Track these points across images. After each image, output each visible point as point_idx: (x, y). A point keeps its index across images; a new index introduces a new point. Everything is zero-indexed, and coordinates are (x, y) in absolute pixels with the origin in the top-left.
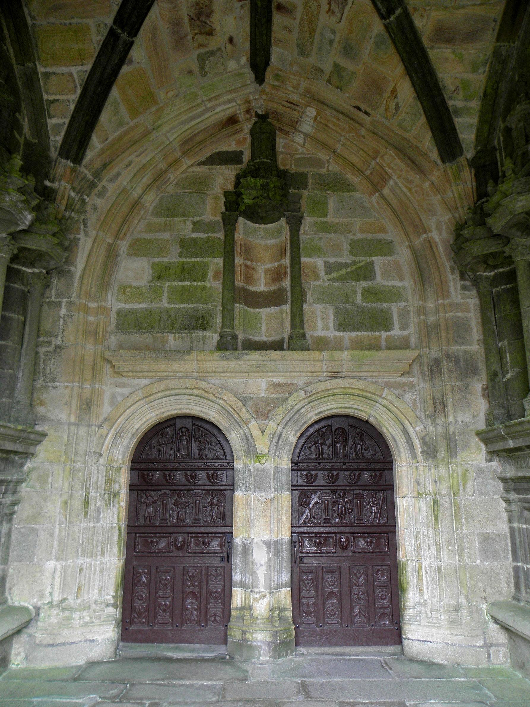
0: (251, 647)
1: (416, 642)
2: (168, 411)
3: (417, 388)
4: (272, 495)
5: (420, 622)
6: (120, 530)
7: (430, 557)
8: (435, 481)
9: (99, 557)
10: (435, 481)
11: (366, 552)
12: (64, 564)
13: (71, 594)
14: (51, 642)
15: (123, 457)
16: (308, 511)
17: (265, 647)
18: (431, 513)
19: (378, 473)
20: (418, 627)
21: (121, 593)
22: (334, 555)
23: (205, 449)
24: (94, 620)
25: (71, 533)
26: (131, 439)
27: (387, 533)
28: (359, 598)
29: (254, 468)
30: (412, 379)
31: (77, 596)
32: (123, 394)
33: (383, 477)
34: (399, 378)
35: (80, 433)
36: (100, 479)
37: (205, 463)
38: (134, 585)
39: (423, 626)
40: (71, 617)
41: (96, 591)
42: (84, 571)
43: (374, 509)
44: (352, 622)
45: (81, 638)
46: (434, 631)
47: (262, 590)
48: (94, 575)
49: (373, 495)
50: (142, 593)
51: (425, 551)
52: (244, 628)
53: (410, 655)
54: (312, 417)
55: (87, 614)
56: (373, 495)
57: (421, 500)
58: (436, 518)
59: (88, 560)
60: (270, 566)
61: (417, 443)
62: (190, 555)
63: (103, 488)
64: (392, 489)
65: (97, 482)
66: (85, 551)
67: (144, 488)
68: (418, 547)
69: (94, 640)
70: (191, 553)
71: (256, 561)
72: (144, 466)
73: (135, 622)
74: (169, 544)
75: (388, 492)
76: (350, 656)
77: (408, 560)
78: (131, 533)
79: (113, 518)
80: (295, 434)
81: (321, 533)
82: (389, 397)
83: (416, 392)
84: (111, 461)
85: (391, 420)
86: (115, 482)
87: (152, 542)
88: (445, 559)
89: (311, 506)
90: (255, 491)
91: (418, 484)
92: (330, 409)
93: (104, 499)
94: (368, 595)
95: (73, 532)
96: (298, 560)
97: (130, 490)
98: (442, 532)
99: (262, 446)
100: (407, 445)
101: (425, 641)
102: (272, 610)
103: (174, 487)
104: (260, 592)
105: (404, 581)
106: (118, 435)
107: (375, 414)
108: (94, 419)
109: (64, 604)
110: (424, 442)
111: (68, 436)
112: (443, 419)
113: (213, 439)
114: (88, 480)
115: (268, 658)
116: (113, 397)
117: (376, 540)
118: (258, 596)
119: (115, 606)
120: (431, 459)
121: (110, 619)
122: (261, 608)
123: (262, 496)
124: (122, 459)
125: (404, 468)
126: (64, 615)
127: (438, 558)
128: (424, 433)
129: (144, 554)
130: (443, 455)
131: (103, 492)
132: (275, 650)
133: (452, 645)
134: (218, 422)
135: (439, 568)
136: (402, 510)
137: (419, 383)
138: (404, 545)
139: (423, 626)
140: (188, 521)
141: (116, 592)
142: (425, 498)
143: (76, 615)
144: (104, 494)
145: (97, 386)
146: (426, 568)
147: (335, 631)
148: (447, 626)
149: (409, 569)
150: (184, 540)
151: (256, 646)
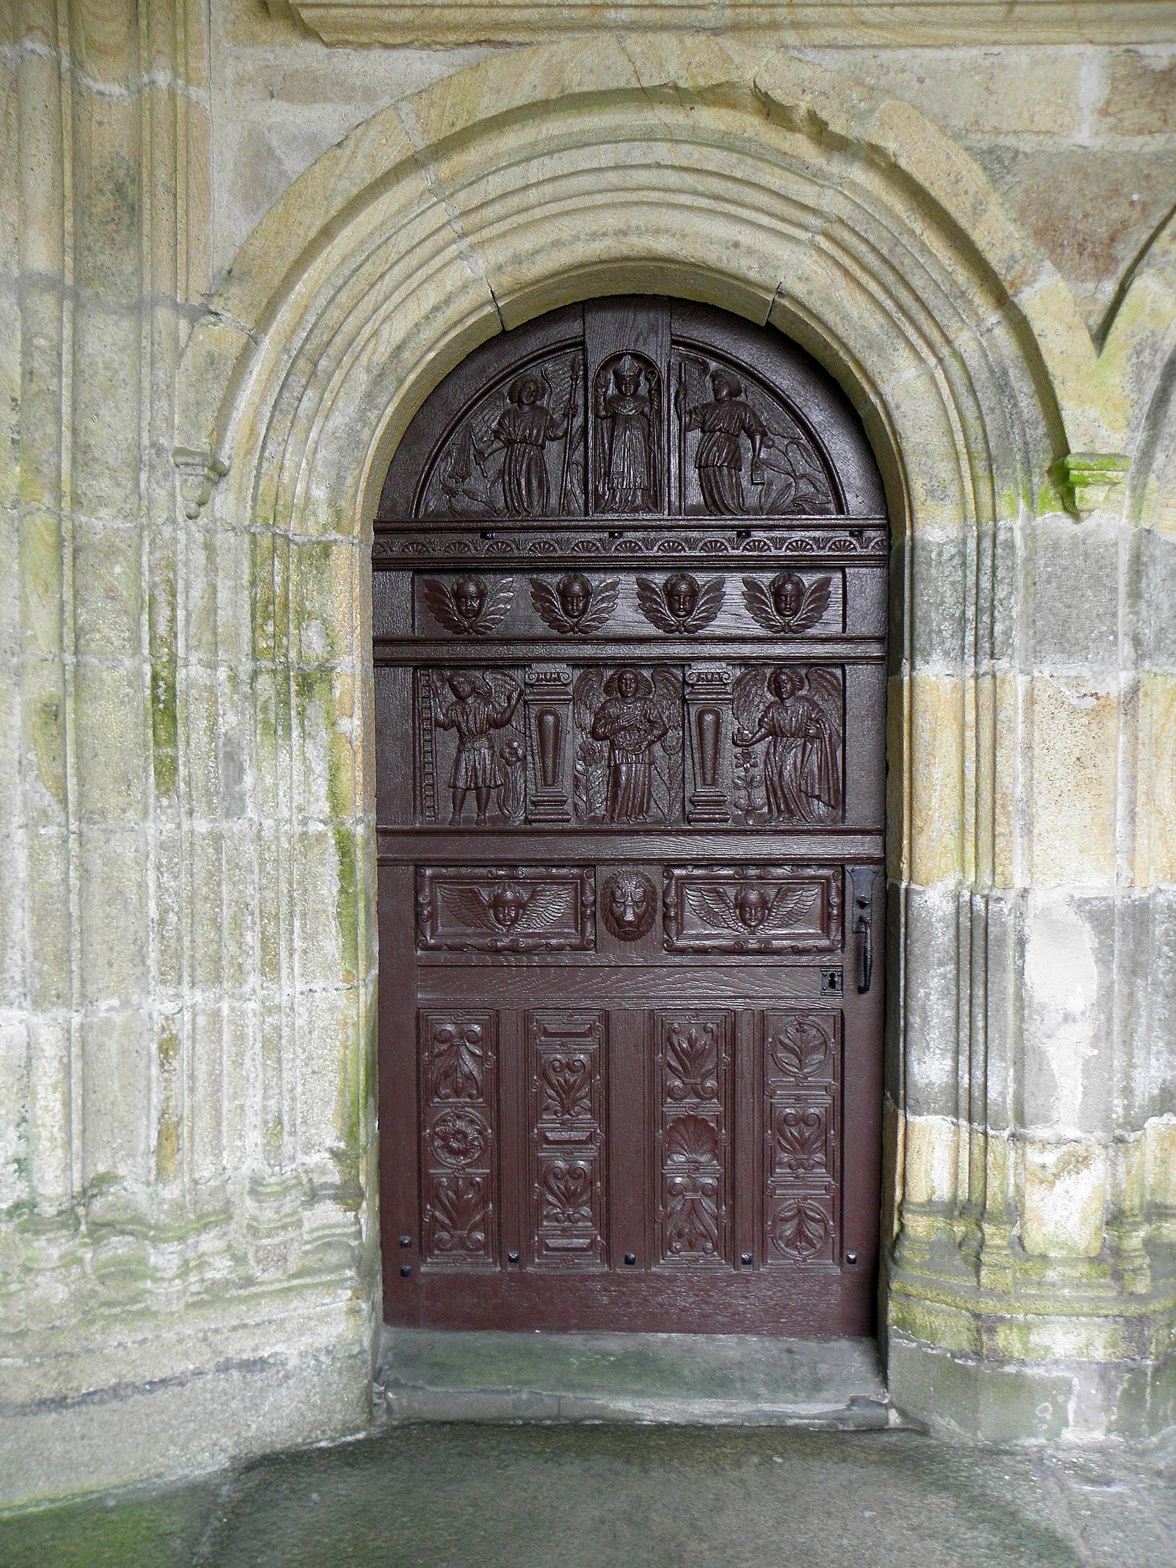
0: (1019, 1384)
2: (556, 244)
6: (345, 848)
9: (253, 980)
12: (77, 1019)
13: (131, 1155)
14: (49, 1390)
15: (336, 490)
17: (1085, 1392)
21: (368, 1129)
23: (735, 463)
24: (257, 1272)
25: (97, 866)
26: (369, 396)
29: (1031, 536)
31: (160, 1170)
32: (313, 140)
35: (92, 346)
36: (223, 596)
37: (744, 532)
38: (425, 1091)
40: (142, 1261)
41: (254, 1137)
42: (185, 1052)
45: (203, 1358)
47: (1072, 1133)
48: (238, 1064)
50: (460, 1124)
52: (987, 1306)
55: (221, 1245)
59: (199, 997)
62: (678, 959)
63: (247, 648)
65: (212, 610)
66: (178, 955)
67: (444, 652)
69: (262, 1361)
70: (682, 951)
72: (439, 546)
73: (439, 1244)
74: (579, 913)
78: (396, 862)
79: (309, 789)
84: (273, 509)
86: (303, 615)
87: (498, 903)
90: (1036, 654)
93: (254, 695)
95: (111, 861)
97: (380, 663)
99: (1093, 413)
102: (1116, 1219)
103: (588, 651)
104: (1059, 1142)
106: (302, 364)
108: (165, 267)
109: (97, 1205)
111: (27, 353)
113: (770, 415)
114: (162, 598)
115: (1098, 1436)
116: (259, 155)
118: (1050, 1158)
119: (347, 1195)
121: (333, 1257)
122: (1064, 1211)
124: (332, 503)
126: (105, 1255)
129: (463, 958)
131: (246, 667)
132: (1133, 1399)
134: (828, 301)
140: (662, 803)
141: (351, 1134)
143: (164, 1258)
144: (255, 674)
145: (163, 78)
150: (649, 896)
151: (1041, 1382)
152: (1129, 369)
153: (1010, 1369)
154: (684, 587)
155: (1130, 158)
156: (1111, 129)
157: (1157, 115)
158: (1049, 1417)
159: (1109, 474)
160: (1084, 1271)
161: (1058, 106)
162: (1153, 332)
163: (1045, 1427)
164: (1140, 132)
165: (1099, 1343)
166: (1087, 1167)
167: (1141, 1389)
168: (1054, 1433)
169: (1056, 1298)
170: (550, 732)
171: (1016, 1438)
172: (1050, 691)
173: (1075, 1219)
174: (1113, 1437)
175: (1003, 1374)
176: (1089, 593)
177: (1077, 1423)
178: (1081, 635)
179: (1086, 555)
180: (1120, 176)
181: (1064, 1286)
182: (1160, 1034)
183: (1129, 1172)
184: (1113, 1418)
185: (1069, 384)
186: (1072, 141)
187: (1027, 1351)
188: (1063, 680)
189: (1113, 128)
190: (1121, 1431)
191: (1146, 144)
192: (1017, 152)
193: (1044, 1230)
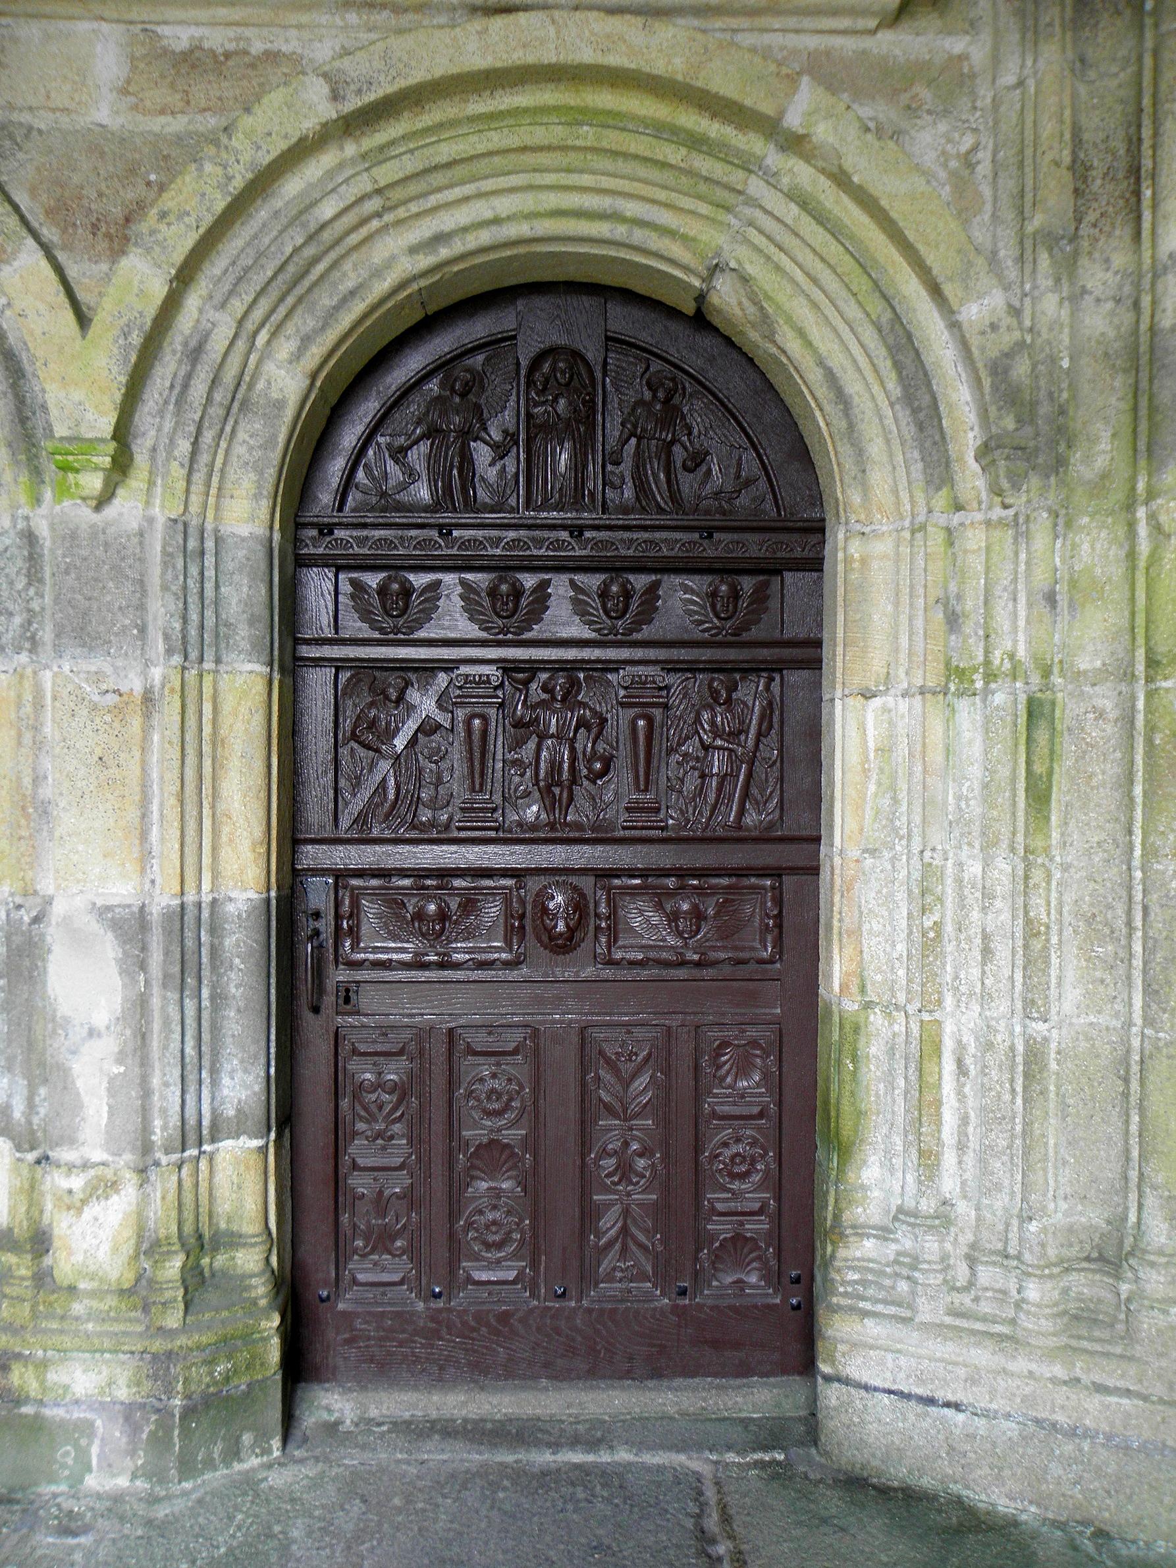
0: (37, 1425)
1: (886, 1399)
3: (985, 95)
4: (157, 673)
5: (910, 1306)
7: (986, 997)
8: (1051, 599)
10: (1051, 599)
11: (667, 964)
16: (385, 766)
17: (108, 1434)
18: (1011, 770)
19: (747, 584)
20: (900, 1331)
22: (514, 975)
27: (776, 873)
28: (625, 1170)
30: (957, 45)
33: (774, 604)
34: (886, 38)
39: (925, 1327)
43: (717, 763)
44: (587, 1277)
46: (982, 1356)
47: (98, 1155)
49: (715, 694)
50: (728, 1153)
51: (960, 965)
53: (849, 1456)
54: (389, 263)
56: (715, 694)
57: (963, 705)
58: (1039, 795)
60: (143, 1037)
61: (960, 399)
64: (816, 664)
68: (929, 945)
70: (359, 965)
71: (64, 1008)
75: (794, 677)
76: (555, 1446)
77: (868, 1006)
80: (297, 356)
81: (445, 874)
82: (822, 132)
83: (975, 119)
85: (826, 277)
88: (1068, 1007)
89: (400, 743)
90: (59, 652)
91: (953, 621)
92: (496, 221)
94: (666, 1157)
96: (329, 1000)
98: (1066, 868)
99: (77, 395)
100: (904, 415)
101: (930, 1401)
102: (149, 1247)
105: (846, 1106)
107: (743, 252)
110: (1002, 386)
112: (1120, 260)
115: (123, 1482)
117: (721, 909)
120: (1035, 481)
123: (97, 677)
125: (882, 547)
127: (1028, 1003)
128: (1007, 339)
130: (1101, 462)
132: (160, 1442)
133: (1072, 1433)
135: (1034, 1056)
136: (854, 759)
137: (996, 60)
138: (856, 933)
139: (925, 1327)
142: (987, 692)
146: (961, 1046)
147: (504, 1317)
148: (1052, 1342)
149: (874, 1049)
151: (62, 1424)
152: (116, 351)
153: (27, 1410)
154: (395, 586)
155: (151, 138)
156: (132, 108)
157: (178, 97)
158: (70, 1462)
159: (95, 459)
160: (113, 1304)
161: (75, 82)
162: (141, 313)
163: (67, 1473)
164: (162, 112)
165: (122, 1381)
166: (117, 1191)
167: (168, 1431)
168: (76, 1480)
169: (76, 1333)
170: (476, 736)
171: (36, 1484)
172: (70, 687)
173: (105, 1248)
174: (138, 1483)
175: (20, 1415)
176: (111, 584)
177: (100, 1468)
178: (102, 628)
179: (106, 544)
180: (137, 156)
181: (88, 1320)
182: (234, 1051)
183: (163, 1198)
184: (140, 1462)
185: (51, 366)
186: (88, 119)
187: (44, 1390)
188: (82, 676)
189: (135, 108)
190: (148, 1477)
191: (168, 124)
192: (30, 128)
193: (73, 1259)
